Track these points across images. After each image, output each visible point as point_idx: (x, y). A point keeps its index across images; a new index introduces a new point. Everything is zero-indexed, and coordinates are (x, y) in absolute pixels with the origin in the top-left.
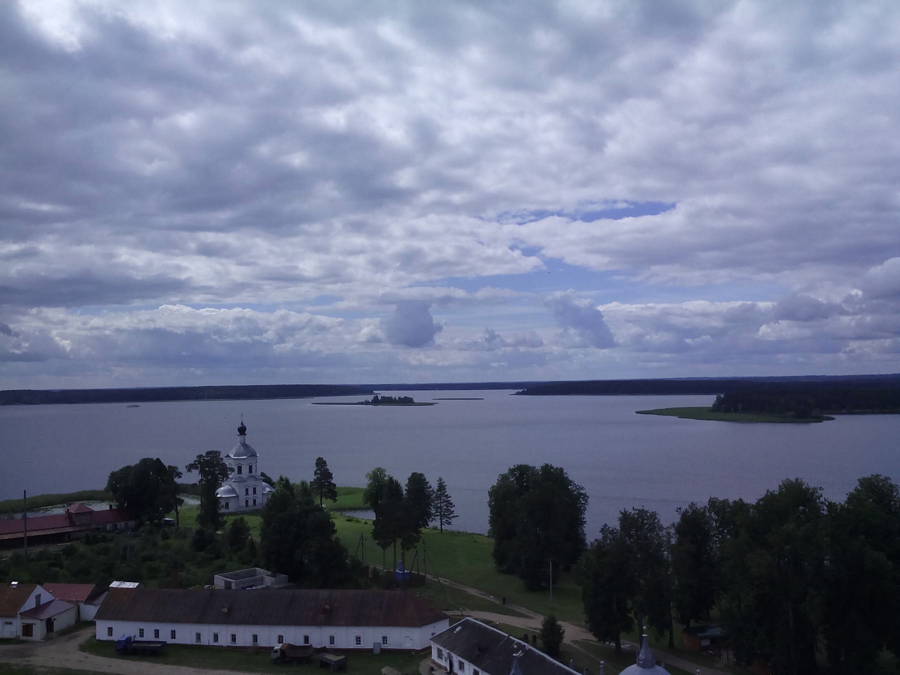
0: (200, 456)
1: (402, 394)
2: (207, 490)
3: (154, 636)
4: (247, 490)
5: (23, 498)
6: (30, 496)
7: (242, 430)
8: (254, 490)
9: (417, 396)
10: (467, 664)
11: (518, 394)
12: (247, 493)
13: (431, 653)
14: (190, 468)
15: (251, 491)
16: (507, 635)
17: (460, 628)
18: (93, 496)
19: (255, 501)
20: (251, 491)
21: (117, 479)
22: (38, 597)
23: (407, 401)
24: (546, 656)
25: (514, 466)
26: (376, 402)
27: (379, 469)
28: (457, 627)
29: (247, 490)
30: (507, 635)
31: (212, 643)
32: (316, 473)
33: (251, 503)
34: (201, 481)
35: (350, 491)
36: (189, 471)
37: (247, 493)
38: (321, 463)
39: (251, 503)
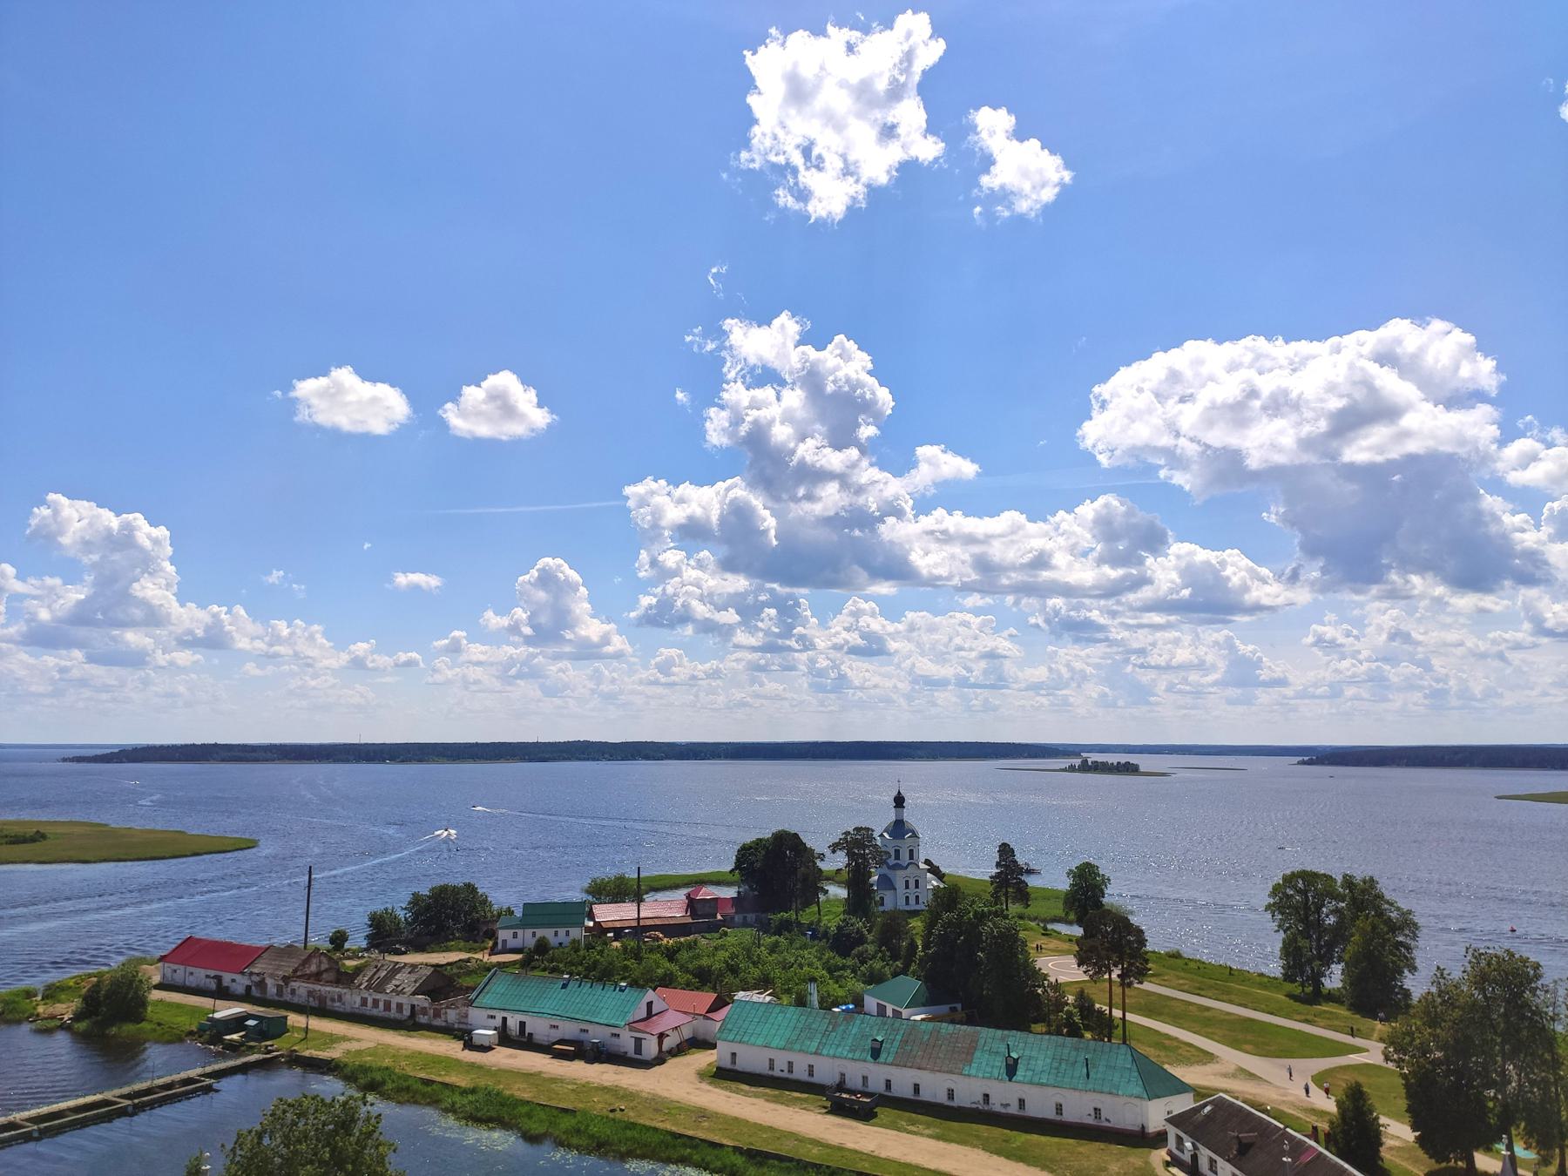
0: (847, 833)
1: (1123, 758)
2: (857, 880)
3: (946, 1097)
4: (907, 882)
5: (636, 876)
6: (647, 874)
7: (899, 801)
8: (917, 881)
9: (1144, 762)
10: (1220, 1162)
11: (1303, 763)
12: (907, 887)
13: (1166, 1140)
14: (835, 848)
15: (912, 884)
16: (1282, 1126)
17: (1208, 1108)
18: (718, 881)
19: (917, 897)
20: (912, 884)
21: (746, 855)
22: (650, 1004)
23: (1130, 769)
24: (1346, 1166)
25: (772, 1068)
26: (1086, 768)
27: (1088, 865)
28: (1205, 1105)
29: (907, 882)
30: (1282, 1126)
31: (785, 1075)
32: (998, 865)
33: (912, 900)
34: (848, 865)
35: (1049, 895)
36: (834, 852)
37: (907, 887)
38: (1006, 851)
39: (912, 900)
